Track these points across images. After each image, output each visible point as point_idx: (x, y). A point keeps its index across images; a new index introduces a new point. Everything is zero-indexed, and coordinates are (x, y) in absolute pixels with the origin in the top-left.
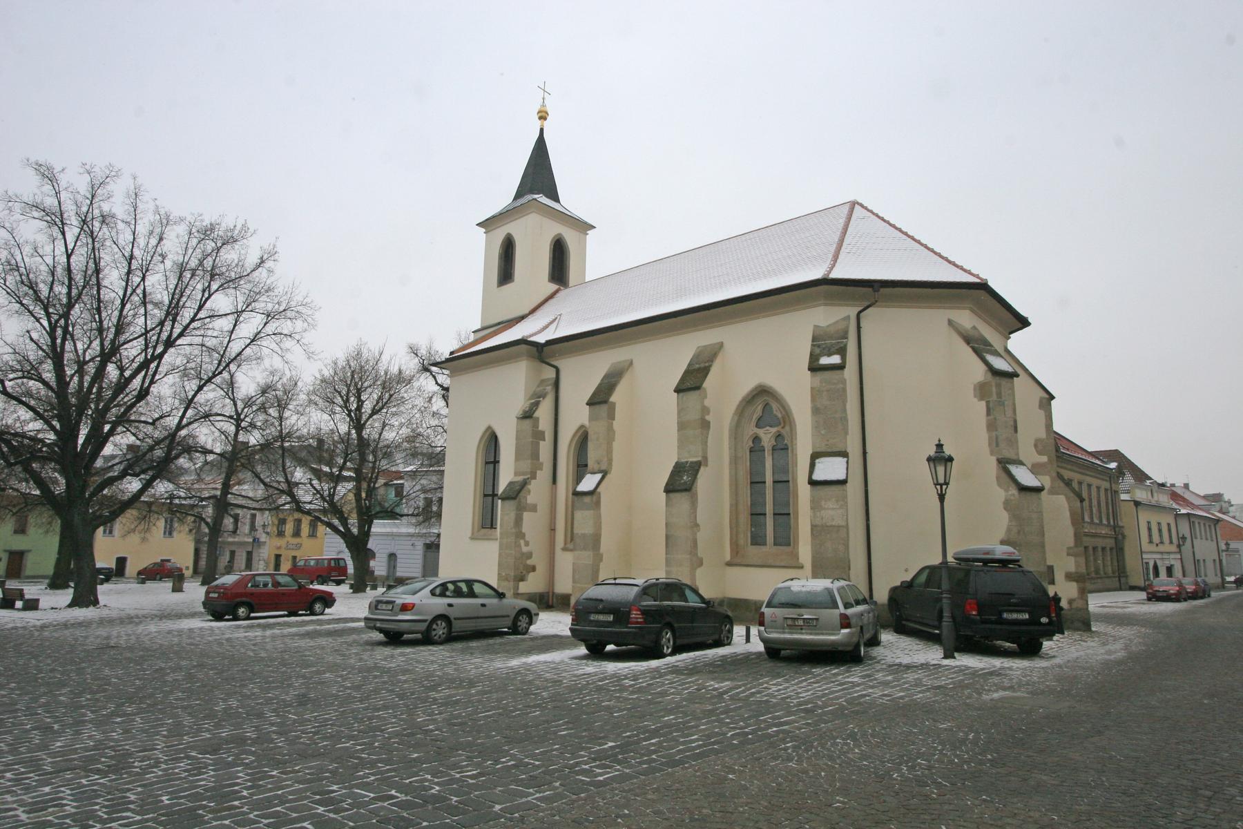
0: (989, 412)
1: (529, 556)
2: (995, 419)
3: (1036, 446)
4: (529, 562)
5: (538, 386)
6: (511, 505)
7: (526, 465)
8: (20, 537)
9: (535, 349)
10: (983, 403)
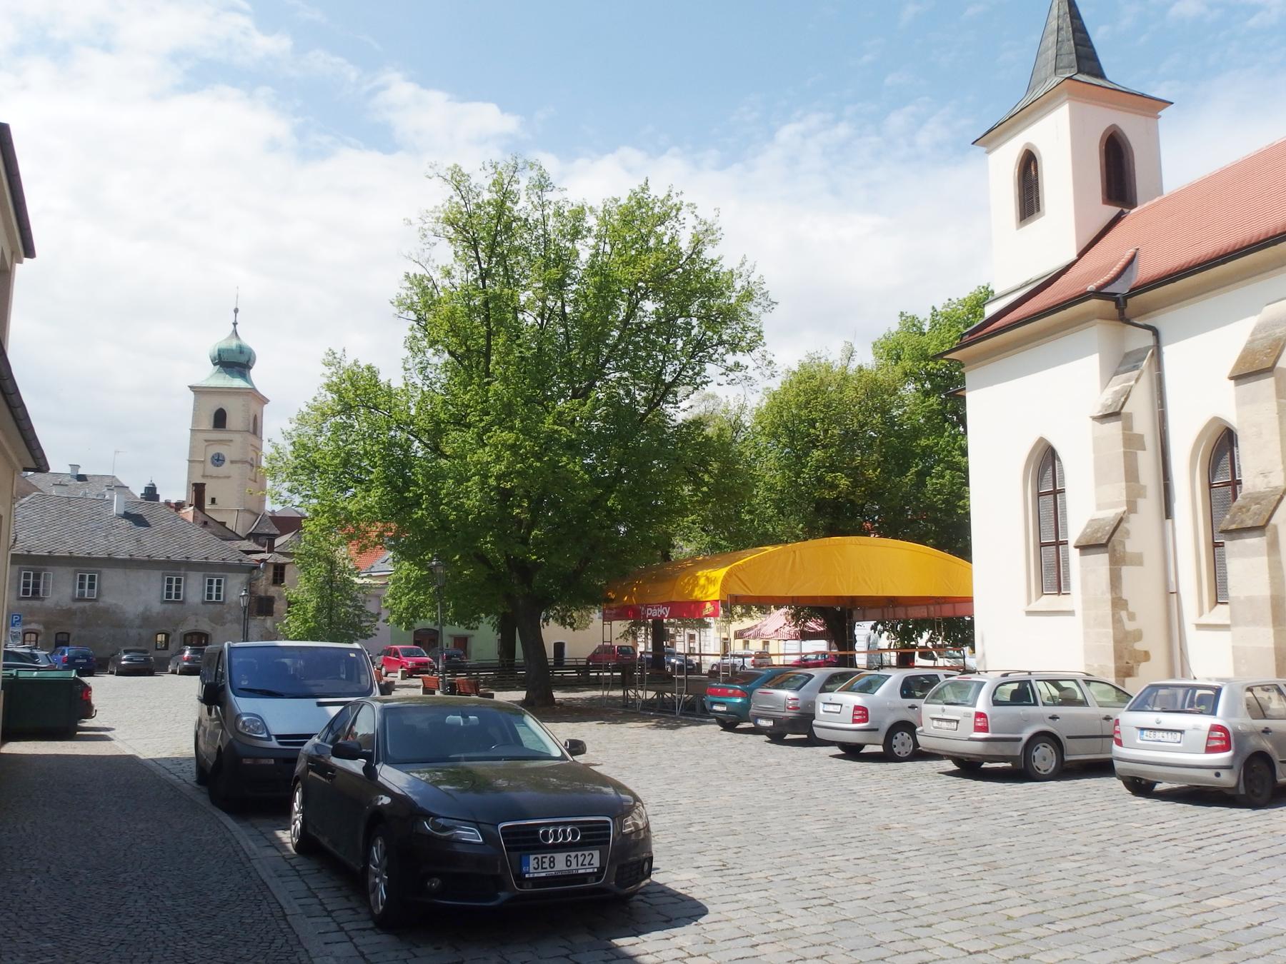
1: (1138, 635)
4: (1140, 646)
5: (1119, 366)
6: (1100, 561)
7: (1117, 492)
8: (1194, 627)
9: (1112, 304)
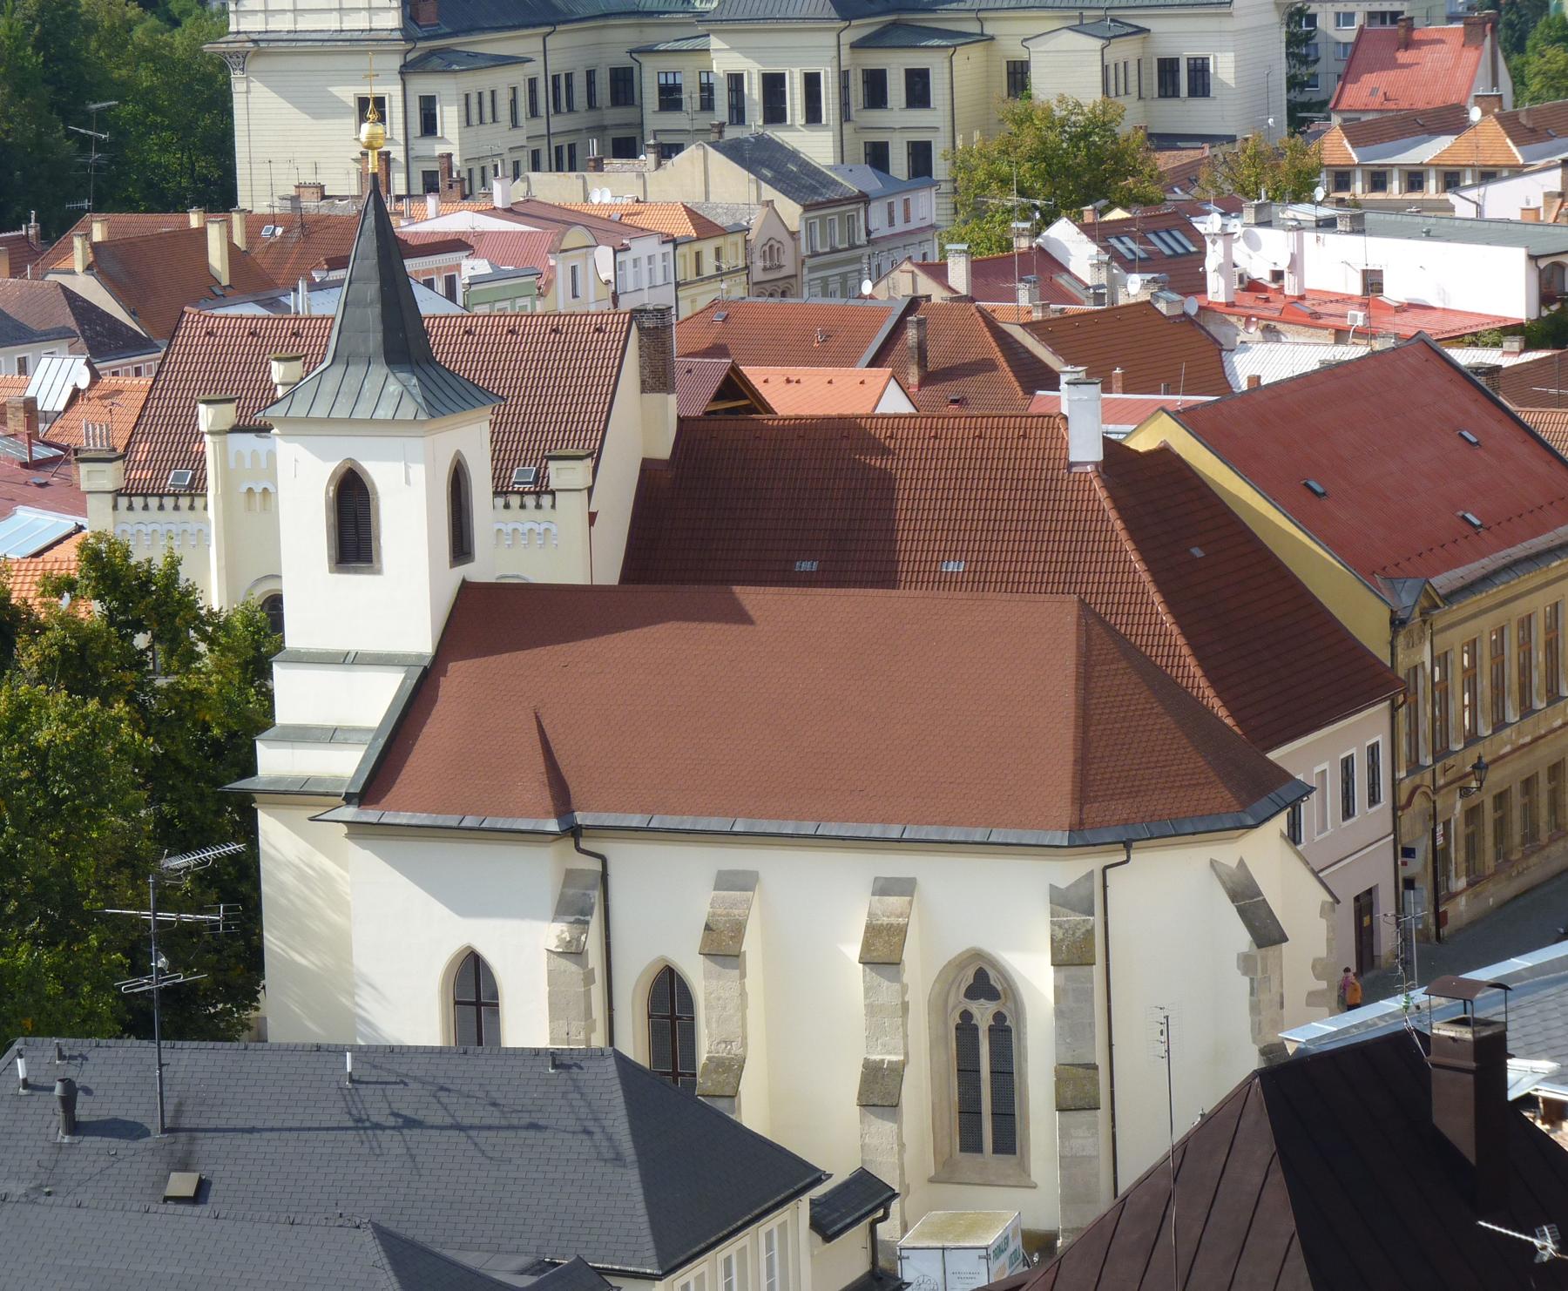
0: (1252, 993)
2: (1259, 1001)
3: (1313, 967)
10: (1247, 980)
